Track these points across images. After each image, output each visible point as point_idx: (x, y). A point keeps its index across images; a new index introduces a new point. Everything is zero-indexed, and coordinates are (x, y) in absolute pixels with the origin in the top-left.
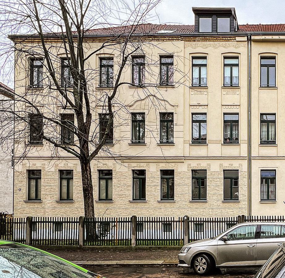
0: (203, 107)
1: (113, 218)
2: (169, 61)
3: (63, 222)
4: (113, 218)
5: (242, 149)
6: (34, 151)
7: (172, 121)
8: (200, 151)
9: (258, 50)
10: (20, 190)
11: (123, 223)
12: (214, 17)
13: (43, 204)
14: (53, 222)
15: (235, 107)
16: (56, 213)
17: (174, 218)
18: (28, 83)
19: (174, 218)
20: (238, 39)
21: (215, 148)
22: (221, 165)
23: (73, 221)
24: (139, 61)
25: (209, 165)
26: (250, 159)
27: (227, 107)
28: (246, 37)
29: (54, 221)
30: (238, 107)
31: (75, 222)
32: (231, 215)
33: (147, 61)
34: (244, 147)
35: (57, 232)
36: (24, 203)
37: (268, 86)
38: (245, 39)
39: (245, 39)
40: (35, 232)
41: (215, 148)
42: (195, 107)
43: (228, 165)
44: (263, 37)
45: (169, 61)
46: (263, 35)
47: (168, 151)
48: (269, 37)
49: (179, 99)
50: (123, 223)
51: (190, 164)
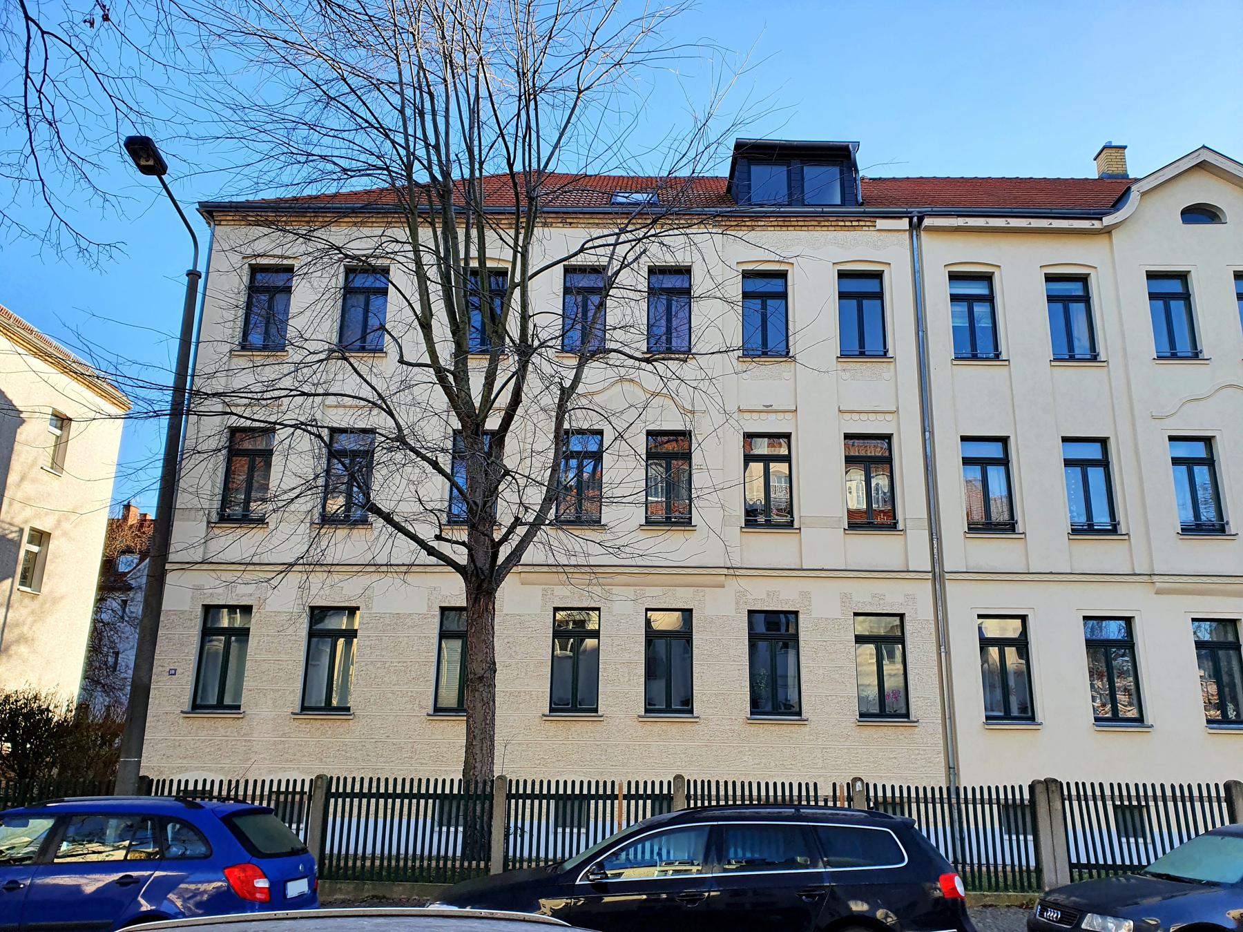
0: (780, 416)
1: (601, 784)
2: (279, 279)
3: (590, 797)
4: (601, 784)
5: (909, 546)
6: (346, 545)
7: (687, 456)
8: (769, 547)
9: (946, 251)
10: (172, 673)
11: (373, 801)
12: (796, 165)
13: (244, 722)
14: (435, 796)
15: (881, 417)
16: (286, 756)
17: (815, 785)
18: (238, 338)
19: (815, 785)
20: (881, 224)
21: (822, 536)
22: (846, 598)
23: (365, 790)
24: (670, 282)
25: (805, 595)
26: (938, 576)
27: (855, 416)
28: (907, 220)
29: (657, 792)
30: (889, 417)
31: (364, 795)
32: (890, 778)
33: (700, 283)
34: (918, 537)
35: (560, 830)
36: (181, 721)
37: (862, 354)
38: (904, 224)
39: (904, 224)
40: (583, 830)
41: (822, 536)
42: (755, 416)
43: (870, 595)
44: (960, 222)
45: (279, 279)
46: (959, 216)
47: (671, 547)
48: (972, 222)
49: (718, 393)
50: (373, 801)
51: (198, 588)
